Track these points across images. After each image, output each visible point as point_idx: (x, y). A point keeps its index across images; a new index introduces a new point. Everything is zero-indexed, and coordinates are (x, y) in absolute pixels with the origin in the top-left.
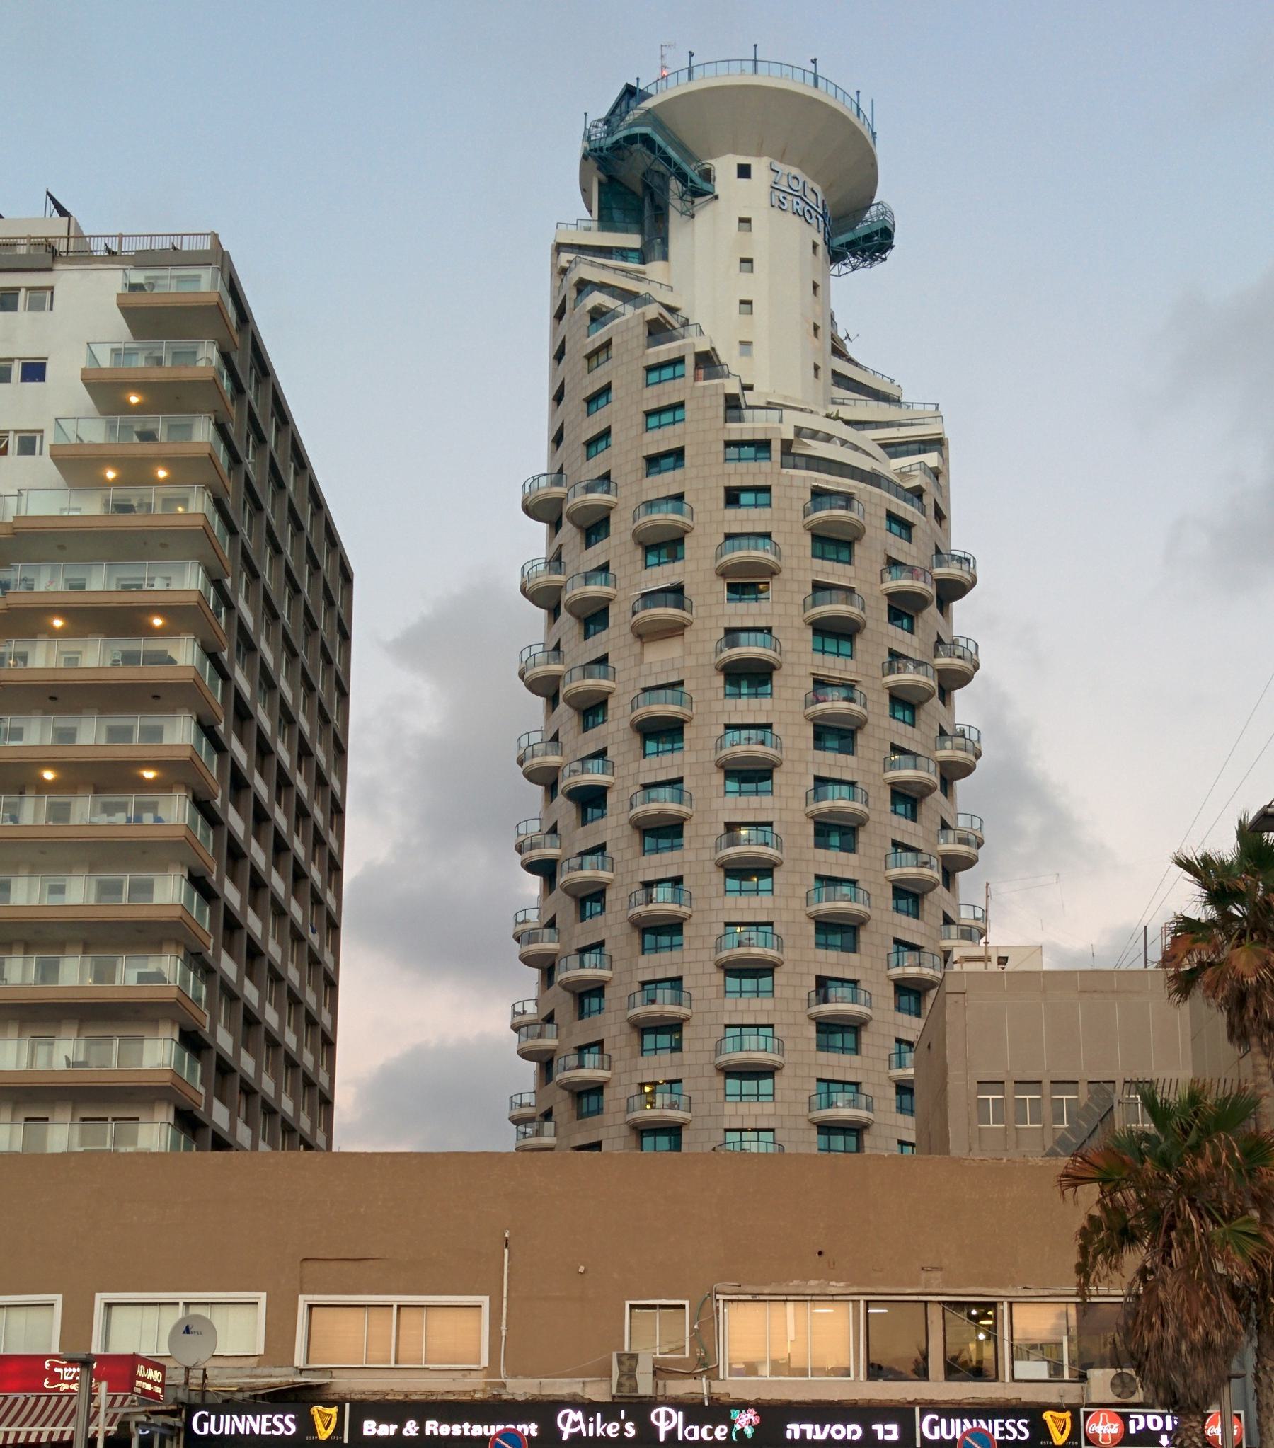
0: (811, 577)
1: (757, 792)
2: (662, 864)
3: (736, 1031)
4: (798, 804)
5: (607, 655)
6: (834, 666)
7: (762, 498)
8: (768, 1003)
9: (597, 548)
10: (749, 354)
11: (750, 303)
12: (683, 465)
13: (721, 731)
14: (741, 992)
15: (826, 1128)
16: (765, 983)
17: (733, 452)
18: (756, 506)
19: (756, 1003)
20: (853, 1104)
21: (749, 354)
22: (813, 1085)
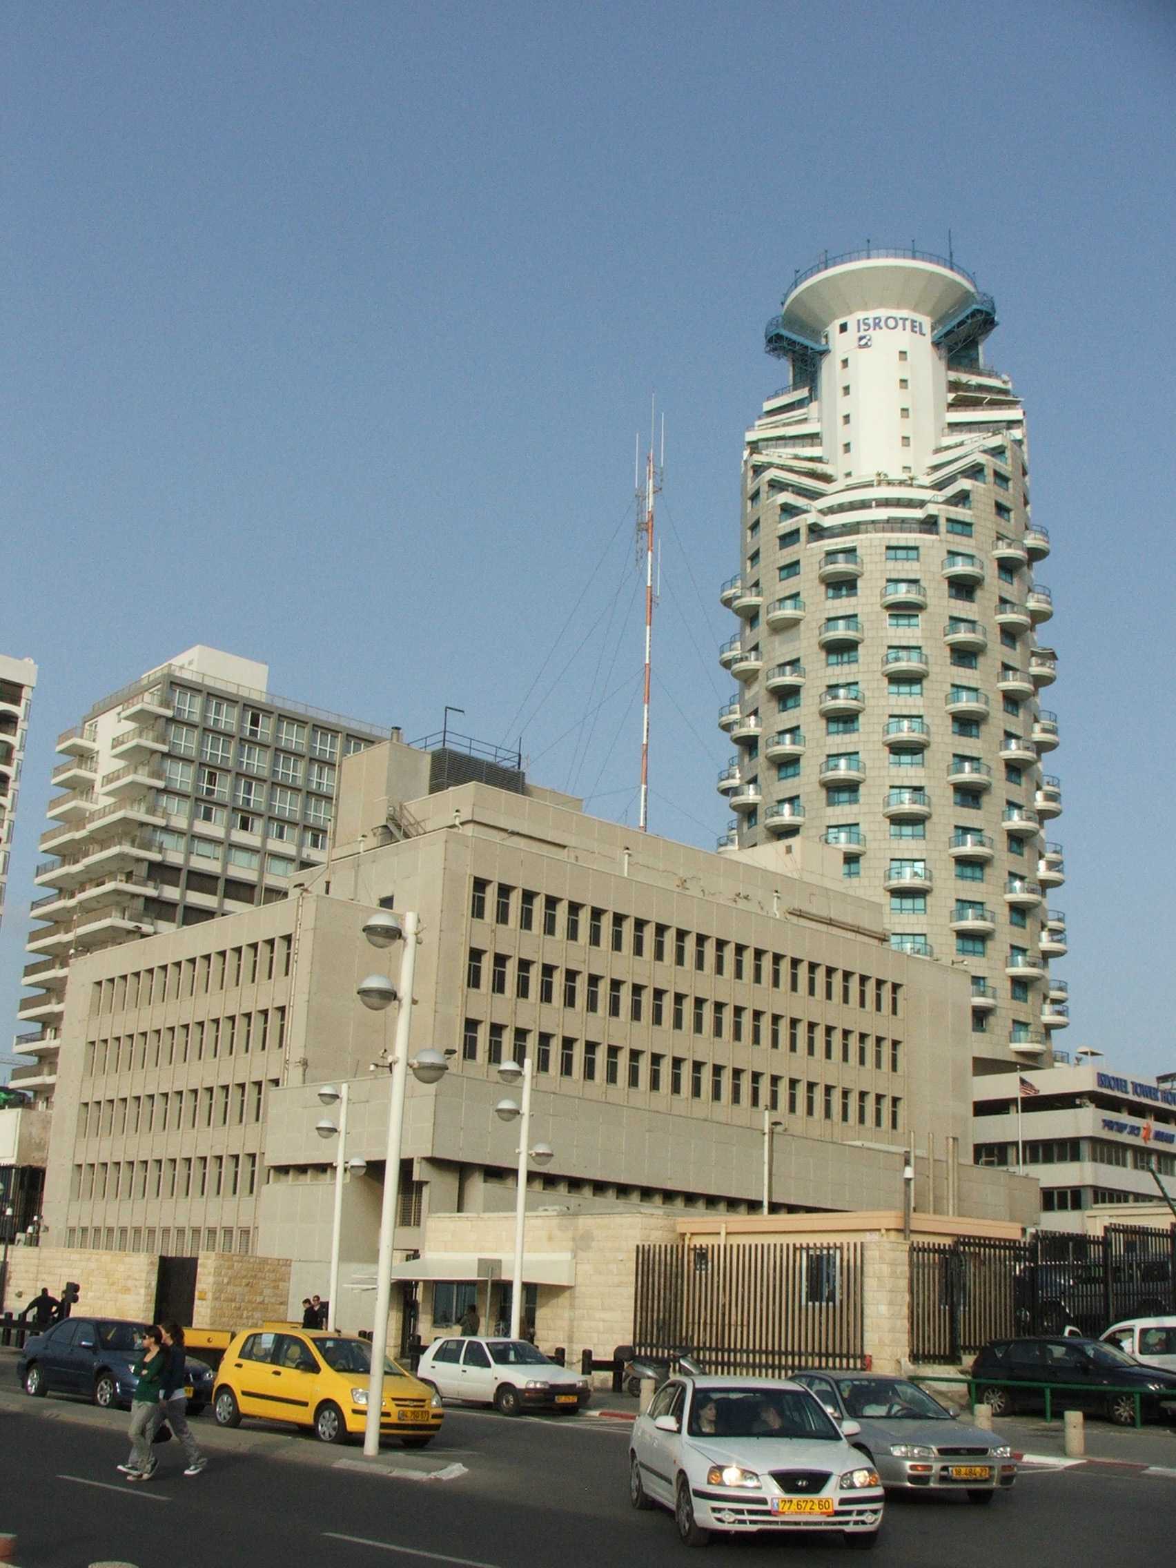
0: (950, 680)
1: (909, 625)
2: (843, 605)
3: (897, 791)
4: (936, 568)
5: (797, 563)
6: (972, 890)
7: (913, 554)
8: (916, 565)
9: (790, 549)
10: (906, 387)
11: (905, 353)
12: (855, 595)
13: (884, 583)
14: (901, 909)
15: (963, 935)
16: (919, 829)
17: (892, 552)
18: (907, 559)
19: (913, 918)
20: (977, 770)
21: (906, 387)
22: (951, 758)
